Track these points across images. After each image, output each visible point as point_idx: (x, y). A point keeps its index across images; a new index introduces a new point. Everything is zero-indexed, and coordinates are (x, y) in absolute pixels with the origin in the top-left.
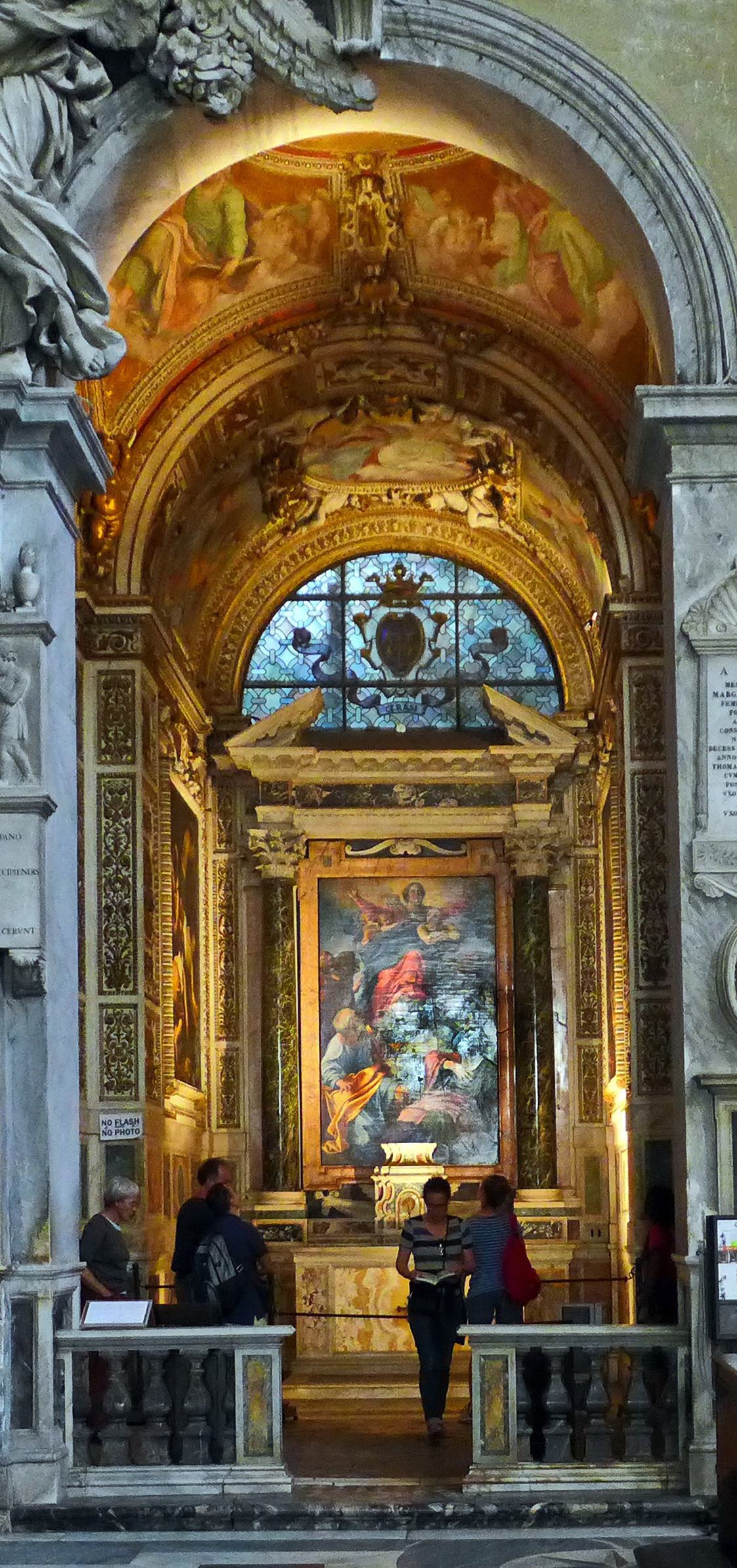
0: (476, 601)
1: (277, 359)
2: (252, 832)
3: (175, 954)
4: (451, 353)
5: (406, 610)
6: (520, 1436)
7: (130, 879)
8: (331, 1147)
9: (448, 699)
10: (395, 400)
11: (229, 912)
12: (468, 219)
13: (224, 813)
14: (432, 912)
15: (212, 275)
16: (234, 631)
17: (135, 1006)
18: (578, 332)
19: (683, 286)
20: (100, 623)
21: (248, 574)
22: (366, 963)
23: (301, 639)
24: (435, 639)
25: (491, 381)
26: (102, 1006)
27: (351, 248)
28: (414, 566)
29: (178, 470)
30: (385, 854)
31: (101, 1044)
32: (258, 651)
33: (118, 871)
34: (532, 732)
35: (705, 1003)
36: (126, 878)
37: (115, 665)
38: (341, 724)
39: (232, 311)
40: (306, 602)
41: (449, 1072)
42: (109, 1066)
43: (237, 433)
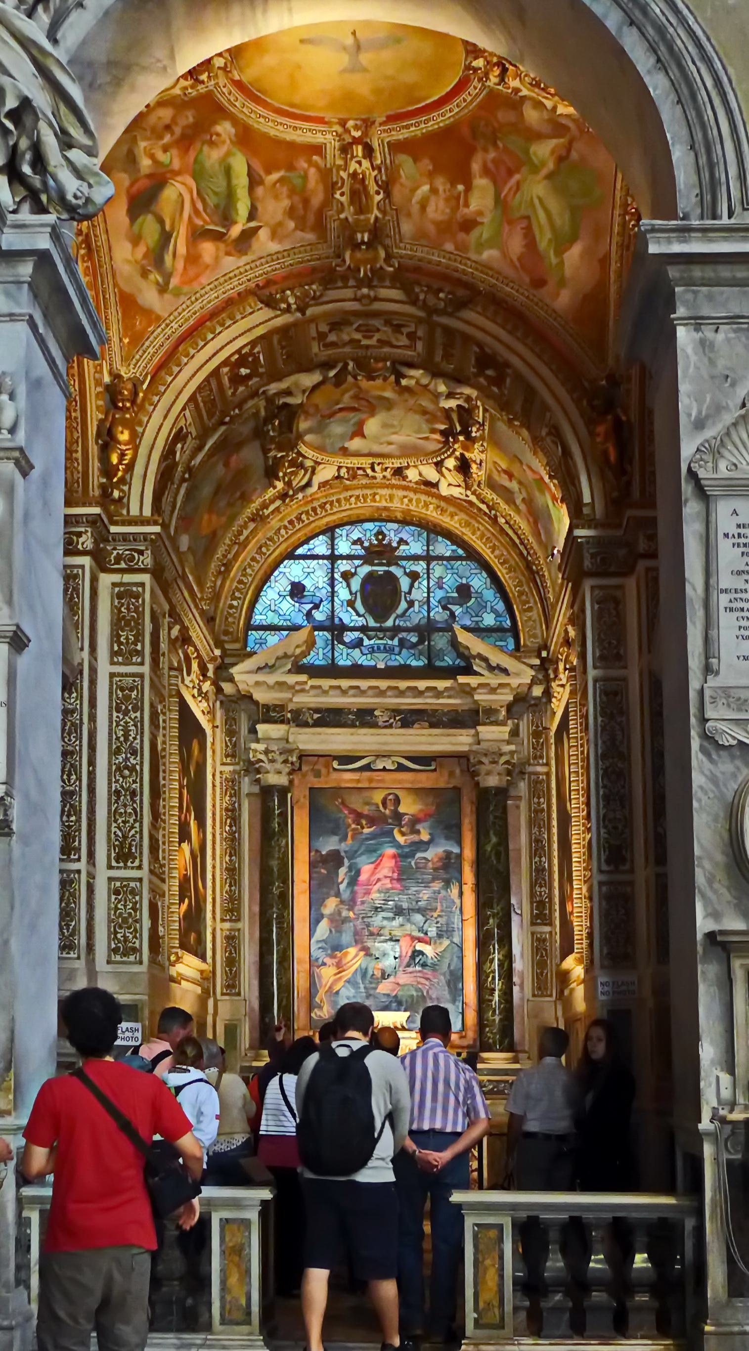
0: (445, 562)
1: (276, 317)
2: (254, 746)
3: (181, 841)
4: (432, 311)
5: (386, 568)
6: (516, 1309)
7: (138, 767)
8: (319, 1013)
9: (421, 642)
10: (380, 365)
11: (233, 815)
12: (448, 186)
13: (231, 733)
14: (406, 818)
15: (219, 237)
16: (240, 582)
17: (140, 880)
18: (544, 293)
19: (685, 132)
20: (114, 540)
21: (253, 532)
22: (349, 860)
23: (297, 590)
24: (410, 593)
25: (467, 339)
26: (110, 879)
27: (342, 216)
28: (392, 533)
29: (187, 413)
30: (367, 768)
31: (109, 914)
32: (260, 601)
33: (127, 759)
34: (494, 665)
35: (720, 858)
36: (134, 766)
37: (128, 578)
38: (330, 662)
39: (237, 272)
40: (301, 561)
41: (421, 953)
42: (116, 933)
43: (241, 389)
